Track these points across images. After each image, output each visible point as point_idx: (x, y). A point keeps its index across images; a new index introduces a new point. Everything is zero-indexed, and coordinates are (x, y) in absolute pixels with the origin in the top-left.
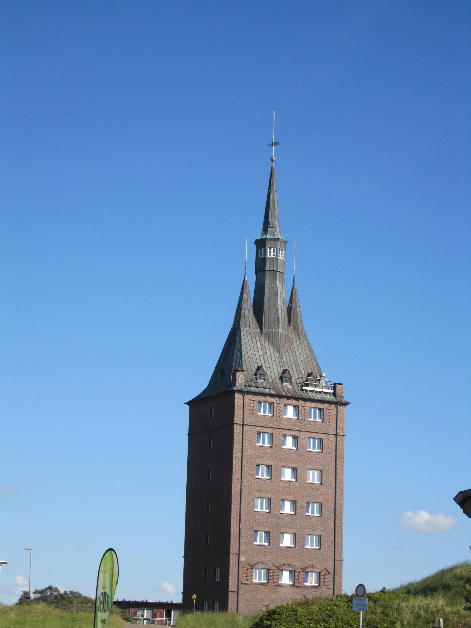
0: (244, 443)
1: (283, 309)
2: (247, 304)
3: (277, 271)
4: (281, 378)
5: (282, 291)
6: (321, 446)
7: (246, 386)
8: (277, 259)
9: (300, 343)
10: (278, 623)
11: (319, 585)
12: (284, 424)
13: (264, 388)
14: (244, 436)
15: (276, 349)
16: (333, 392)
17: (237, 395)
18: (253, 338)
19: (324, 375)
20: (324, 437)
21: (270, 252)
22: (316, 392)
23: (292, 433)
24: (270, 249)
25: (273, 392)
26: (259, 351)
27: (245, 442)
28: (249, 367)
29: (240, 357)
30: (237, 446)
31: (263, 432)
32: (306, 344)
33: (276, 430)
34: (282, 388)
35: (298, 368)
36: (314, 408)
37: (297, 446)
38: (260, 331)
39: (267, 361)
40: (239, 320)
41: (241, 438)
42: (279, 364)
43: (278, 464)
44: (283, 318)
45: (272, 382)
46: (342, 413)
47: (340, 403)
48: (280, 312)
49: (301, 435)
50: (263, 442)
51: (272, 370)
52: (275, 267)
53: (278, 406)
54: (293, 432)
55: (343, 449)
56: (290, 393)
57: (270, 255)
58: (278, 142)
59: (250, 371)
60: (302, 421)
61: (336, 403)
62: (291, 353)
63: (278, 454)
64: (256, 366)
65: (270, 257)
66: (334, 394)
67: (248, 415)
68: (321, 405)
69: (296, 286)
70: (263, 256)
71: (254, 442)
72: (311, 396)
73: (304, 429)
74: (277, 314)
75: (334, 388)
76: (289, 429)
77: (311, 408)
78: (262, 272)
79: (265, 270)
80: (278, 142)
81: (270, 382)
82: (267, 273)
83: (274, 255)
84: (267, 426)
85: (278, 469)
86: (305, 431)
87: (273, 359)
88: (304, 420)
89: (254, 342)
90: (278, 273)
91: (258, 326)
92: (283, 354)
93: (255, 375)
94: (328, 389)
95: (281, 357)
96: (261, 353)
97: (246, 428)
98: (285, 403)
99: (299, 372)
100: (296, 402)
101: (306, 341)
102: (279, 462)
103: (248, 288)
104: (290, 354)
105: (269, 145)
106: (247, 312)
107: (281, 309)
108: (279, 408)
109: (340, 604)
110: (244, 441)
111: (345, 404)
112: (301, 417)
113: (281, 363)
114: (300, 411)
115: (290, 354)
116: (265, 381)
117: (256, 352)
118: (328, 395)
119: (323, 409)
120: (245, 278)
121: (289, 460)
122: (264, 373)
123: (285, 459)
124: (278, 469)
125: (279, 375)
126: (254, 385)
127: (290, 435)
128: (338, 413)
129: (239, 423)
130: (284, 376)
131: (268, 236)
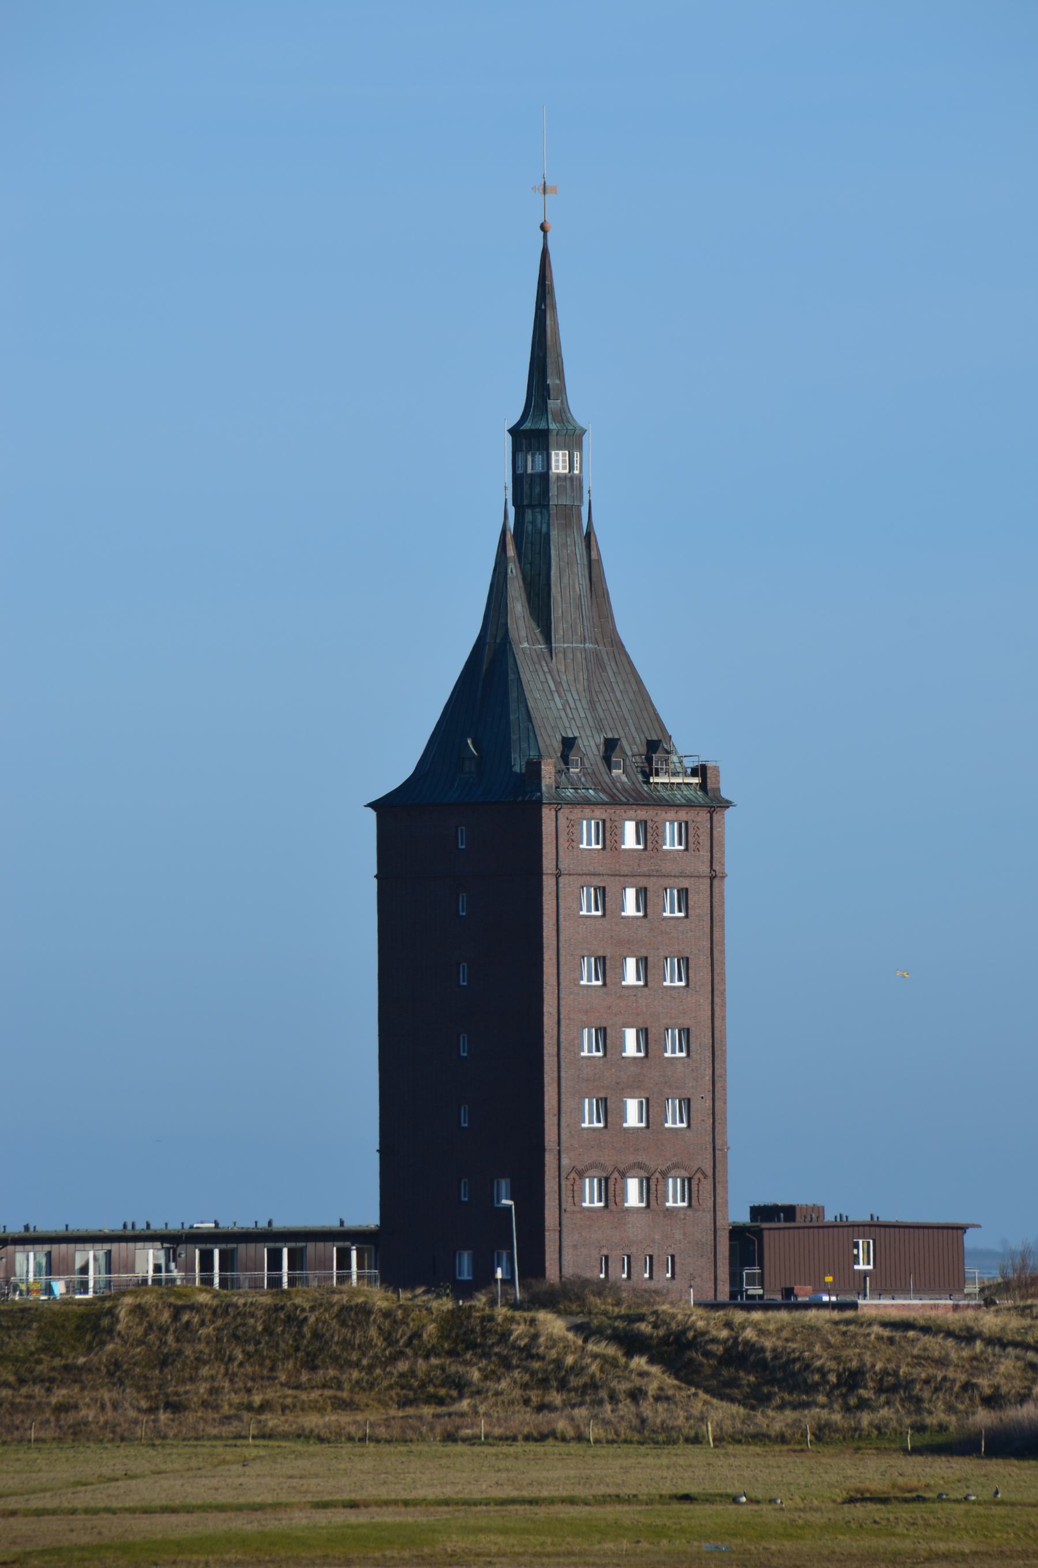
11: (648, 1206)
35: (627, 731)
66: (703, 786)
91: (540, 637)
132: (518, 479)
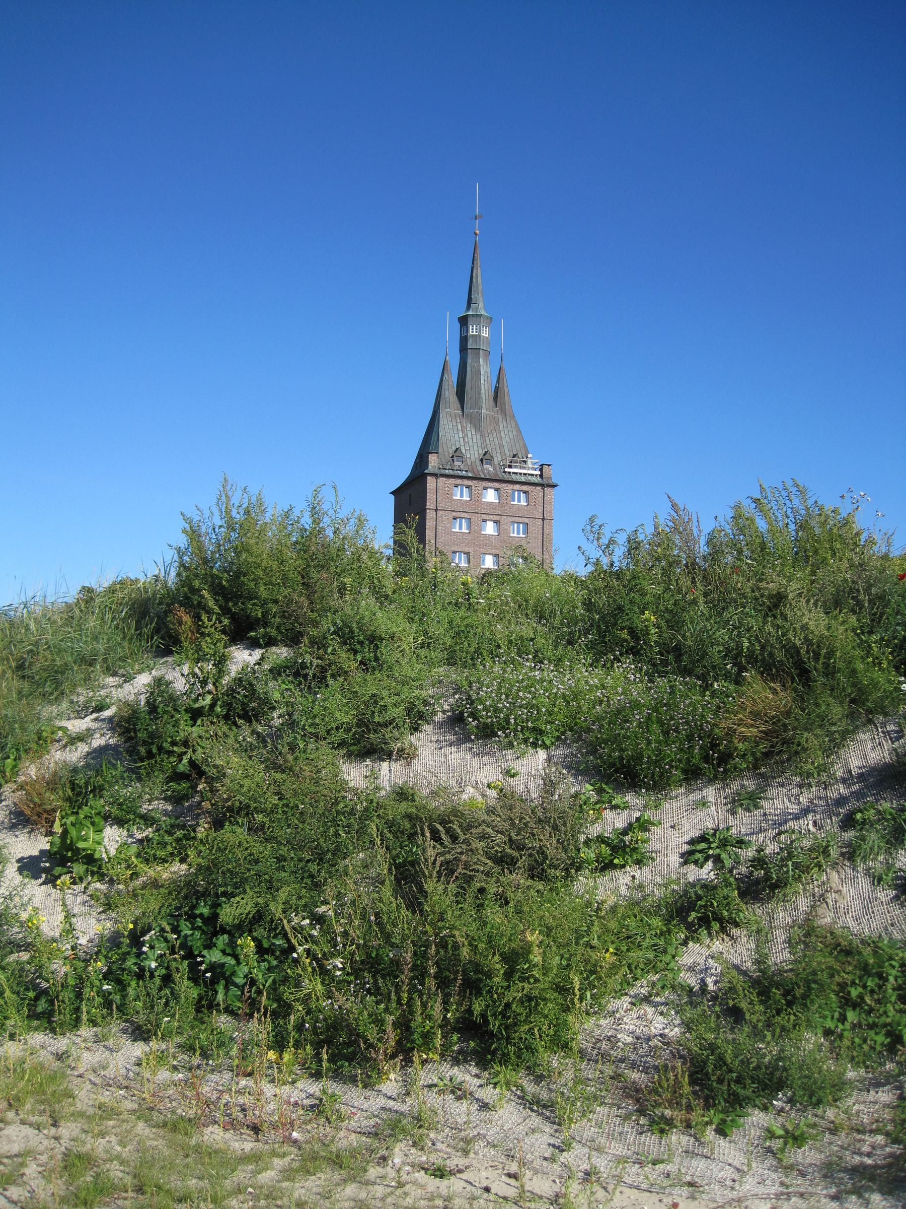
4: (482, 460)
6: (526, 531)
19: (530, 456)
23: (493, 517)
25: (470, 475)
28: (446, 449)
32: (513, 425)
48: (483, 391)
49: (503, 519)
50: (460, 528)
56: (490, 475)
59: (446, 454)
61: (542, 485)
64: (454, 449)
66: (541, 476)
68: (525, 488)
69: (503, 366)
74: (480, 393)
75: (541, 470)
77: (514, 490)
82: (470, 351)
93: (452, 457)
95: (483, 438)
97: (440, 513)
99: (502, 453)
106: (447, 393)
109: (108, 1171)
130: (456, 454)
131: (470, 313)
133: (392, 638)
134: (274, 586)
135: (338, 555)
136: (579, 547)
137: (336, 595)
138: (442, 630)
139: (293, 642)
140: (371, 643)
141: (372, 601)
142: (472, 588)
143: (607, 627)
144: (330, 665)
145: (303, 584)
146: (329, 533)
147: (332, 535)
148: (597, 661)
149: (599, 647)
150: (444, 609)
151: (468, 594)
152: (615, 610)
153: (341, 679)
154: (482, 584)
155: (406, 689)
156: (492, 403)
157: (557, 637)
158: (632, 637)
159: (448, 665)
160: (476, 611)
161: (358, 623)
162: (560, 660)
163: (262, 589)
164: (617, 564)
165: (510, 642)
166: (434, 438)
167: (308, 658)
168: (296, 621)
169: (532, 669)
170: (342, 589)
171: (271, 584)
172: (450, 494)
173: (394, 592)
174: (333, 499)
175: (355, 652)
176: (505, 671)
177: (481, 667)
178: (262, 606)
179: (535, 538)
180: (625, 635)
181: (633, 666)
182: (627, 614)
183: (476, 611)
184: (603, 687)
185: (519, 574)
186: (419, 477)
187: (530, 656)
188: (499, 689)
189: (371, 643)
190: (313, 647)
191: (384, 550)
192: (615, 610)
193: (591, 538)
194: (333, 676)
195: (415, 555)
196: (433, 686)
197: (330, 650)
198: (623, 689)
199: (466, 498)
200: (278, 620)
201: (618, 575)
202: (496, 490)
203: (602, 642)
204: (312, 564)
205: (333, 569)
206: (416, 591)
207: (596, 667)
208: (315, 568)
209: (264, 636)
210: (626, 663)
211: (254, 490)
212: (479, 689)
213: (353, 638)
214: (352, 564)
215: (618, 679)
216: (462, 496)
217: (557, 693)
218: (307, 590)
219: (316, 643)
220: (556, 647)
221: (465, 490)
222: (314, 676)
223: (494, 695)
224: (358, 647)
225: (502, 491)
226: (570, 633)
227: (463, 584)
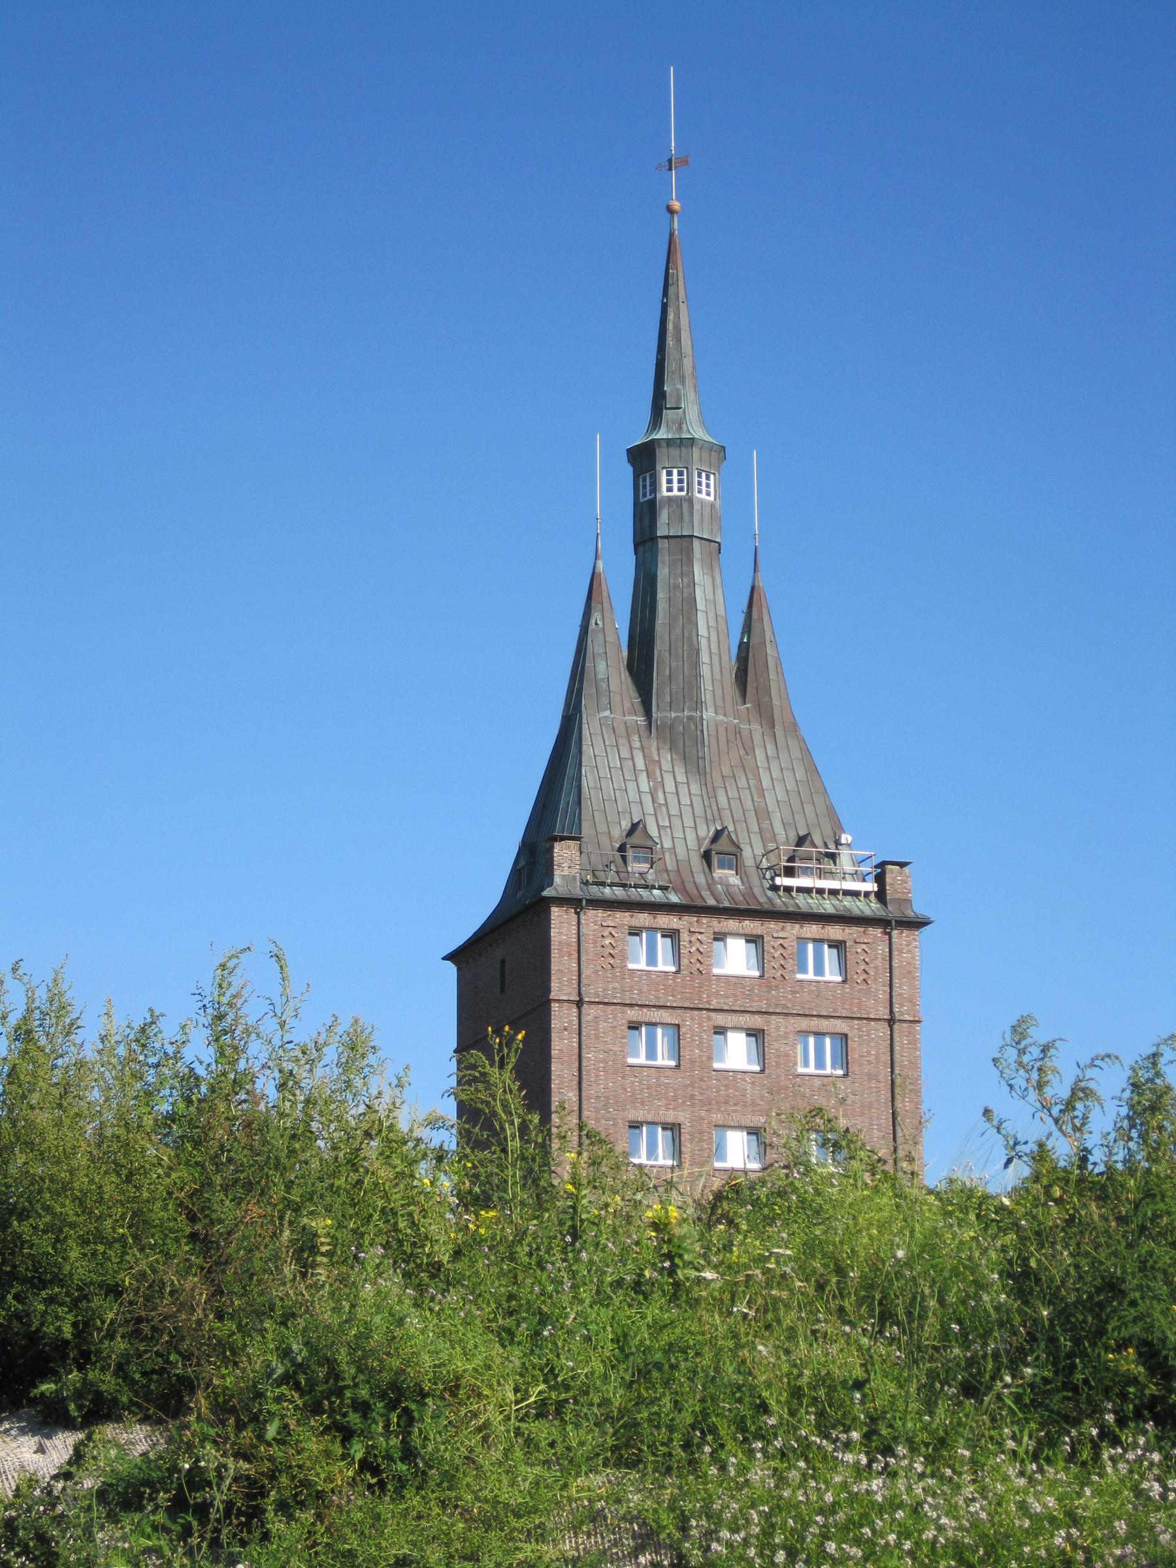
0: (584, 1060)
1: (715, 649)
2: (602, 642)
3: (692, 536)
4: (707, 856)
5: (710, 596)
6: (844, 1058)
7: (586, 883)
8: (690, 500)
9: (775, 752)
10: (974, 1506)
12: (717, 994)
13: (646, 887)
14: (583, 1038)
15: (695, 770)
16: (876, 889)
17: (555, 911)
18: (622, 741)
19: (845, 838)
20: (852, 1027)
21: (669, 481)
22: (820, 891)
24: (669, 474)
25: (674, 898)
26: (639, 780)
27: (588, 1055)
28: (602, 828)
29: (576, 799)
30: (562, 1070)
31: (647, 1024)
32: (796, 753)
33: (689, 1014)
34: (708, 885)
36: (815, 940)
37: (845, 1066)
38: (645, 721)
39: (664, 809)
40: (580, 690)
41: (576, 1045)
42: (703, 815)
43: (702, 1118)
44: (717, 676)
45: (676, 868)
46: (909, 952)
47: (896, 921)
48: (705, 657)
49: (774, 1025)
51: (678, 834)
52: (685, 525)
53: (693, 939)
54: (747, 1017)
55: (914, 1064)
56: (730, 896)
57: (670, 489)
58: (687, 157)
59: (604, 841)
60: (774, 982)
62: (744, 779)
63: (700, 1088)
64: (626, 825)
65: (670, 498)
66: (881, 895)
67: (596, 972)
68: (835, 932)
69: (761, 583)
70: (649, 497)
71: (618, 1053)
72: (801, 905)
73: (784, 1007)
74: (696, 664)
75: (880, 879)
76: (733, 1008)
77: (802, 940)
78: (648, 545)
79: (657, 537)
80: (687, 157)
81: (669, 869)
82: (663, 545)
83: (680, 489)
84: (661, 1004)
85: (701, 1133)
86: (786, 1014)
87: (685, 800)
88: (780, 978)
89: (625, 753)
90: (696, 544)
92: (718, 783)
93: (622, 849)
94: (864, 880)
96: (644, 785)
97: (590, 1012)
98: (717, 930)
100: (751, 926)
101: (797, 743)
102: (703, 1114)
103: (605, 594)
104: (742, 783)
105: (659, 168)
106: (601, 666)
107: (708, 651)
108: (698, 945)
110: (584, 1051)
111: (917, 924)
112: (773, 971)
113: (708, 811)
114: (769, 952)
115: (742, 783)
116: (651, 867)
117: (627, 782)
118: (862, 898)
119: (845, 942)
120: (598, 565)
121: (735, 1105)
122: (649, 844)
123: (723, 1101)
124: (701, 1133)
125: (700, 848)
126: (612, 878)
127: (736, 1028)
128: (895, 953)
129: (565, 998)
131: (662, 434)
132: (637, 504)
133: (454, 1390)
134: (110, 1245)
135: (292, 1152)
136: (987, 1112)
137: (289, 1269)
138: (597, 1365)
139: (164, 1408)
140: (392, 1406)
141: (392, 1282)
142: (683, 1238)
143: (1077, 1342)
144: (272, 1477)
145: (193, 1237)
146: (267, 1086)
147: (272, 1094)
148: (1052, 1442)
149: (1055, 1402)
150: (601, 1299)
151: (669, 1256)
152: (1099, 1290)
153: (307, 1516)
154: (709, 1226)
155: (494, 1539)
156: (731, 690)
157: (932, 1375)
158: (1152, 1370)
159: (617, 1465)
160: (694, 1303)
161: (352, 1350)
162: (942, 1442)
163: (74, 1254)
164: (1097, 1156)
165: (796, 1393)
166: (566, 798)
167: (210, 1457)
168: (173, 1345)
169: (866, 1471)
170: (306, 1248)
171: (100, 1238)
172: (615, 958)
173: (457, 1254)
174: (275, 992)
175: (347, 1435)
176: (781, 1481)
177: (713, 1471)
178: (75, 1305)
179: (871, 1077)
180: (1129, 1363)
181: (1156, 1457)
182: (1133, 1303)
183: (694, 1303)
184: (1073, 1519)
185: (818, 1192)
186: (527, 908)
187: (855, 1435)
188: (768, 1531)
189: (392, 1406)
190: (223, 1422)
191: (424, 1133)
192: (1099, 1290)
193: (1020, 1082)
194: (283, 1507)
195: (514, 1145)
196: (575, 1529)
197: (272, 1430)
198: (1131, 1525)
199: (665, 965)
200: (120, 1345)
201: (1103, 1188)
202: (753, 939)
203: (1065, 1386)
204: (218, 1180)
205: (277, 1192)
206: (522, 1251)
207: (1048, 1461)
208: (225, 1188)
209: (79, 1395)
210: (1135, 1445)
211: (39, 973)
212: (710, 1535)
213: (339, 1392)
214: (334, 1175)
215: (1116, 1494)
216: (652, 959)
217: (935, 1540)
218: (205, 1253)
219: (233, 1410)
220: (930, 1410)
221: (663, 944)
222: (229, 1505)
223: (752, 1552)
224: (354, 1419)
225: (769, 942)
226: (971, 1362)
227: (656, 1226)
